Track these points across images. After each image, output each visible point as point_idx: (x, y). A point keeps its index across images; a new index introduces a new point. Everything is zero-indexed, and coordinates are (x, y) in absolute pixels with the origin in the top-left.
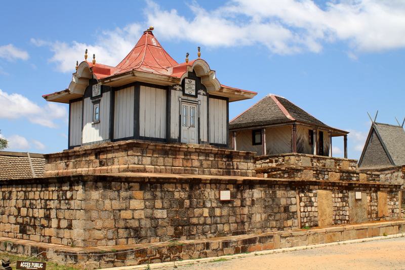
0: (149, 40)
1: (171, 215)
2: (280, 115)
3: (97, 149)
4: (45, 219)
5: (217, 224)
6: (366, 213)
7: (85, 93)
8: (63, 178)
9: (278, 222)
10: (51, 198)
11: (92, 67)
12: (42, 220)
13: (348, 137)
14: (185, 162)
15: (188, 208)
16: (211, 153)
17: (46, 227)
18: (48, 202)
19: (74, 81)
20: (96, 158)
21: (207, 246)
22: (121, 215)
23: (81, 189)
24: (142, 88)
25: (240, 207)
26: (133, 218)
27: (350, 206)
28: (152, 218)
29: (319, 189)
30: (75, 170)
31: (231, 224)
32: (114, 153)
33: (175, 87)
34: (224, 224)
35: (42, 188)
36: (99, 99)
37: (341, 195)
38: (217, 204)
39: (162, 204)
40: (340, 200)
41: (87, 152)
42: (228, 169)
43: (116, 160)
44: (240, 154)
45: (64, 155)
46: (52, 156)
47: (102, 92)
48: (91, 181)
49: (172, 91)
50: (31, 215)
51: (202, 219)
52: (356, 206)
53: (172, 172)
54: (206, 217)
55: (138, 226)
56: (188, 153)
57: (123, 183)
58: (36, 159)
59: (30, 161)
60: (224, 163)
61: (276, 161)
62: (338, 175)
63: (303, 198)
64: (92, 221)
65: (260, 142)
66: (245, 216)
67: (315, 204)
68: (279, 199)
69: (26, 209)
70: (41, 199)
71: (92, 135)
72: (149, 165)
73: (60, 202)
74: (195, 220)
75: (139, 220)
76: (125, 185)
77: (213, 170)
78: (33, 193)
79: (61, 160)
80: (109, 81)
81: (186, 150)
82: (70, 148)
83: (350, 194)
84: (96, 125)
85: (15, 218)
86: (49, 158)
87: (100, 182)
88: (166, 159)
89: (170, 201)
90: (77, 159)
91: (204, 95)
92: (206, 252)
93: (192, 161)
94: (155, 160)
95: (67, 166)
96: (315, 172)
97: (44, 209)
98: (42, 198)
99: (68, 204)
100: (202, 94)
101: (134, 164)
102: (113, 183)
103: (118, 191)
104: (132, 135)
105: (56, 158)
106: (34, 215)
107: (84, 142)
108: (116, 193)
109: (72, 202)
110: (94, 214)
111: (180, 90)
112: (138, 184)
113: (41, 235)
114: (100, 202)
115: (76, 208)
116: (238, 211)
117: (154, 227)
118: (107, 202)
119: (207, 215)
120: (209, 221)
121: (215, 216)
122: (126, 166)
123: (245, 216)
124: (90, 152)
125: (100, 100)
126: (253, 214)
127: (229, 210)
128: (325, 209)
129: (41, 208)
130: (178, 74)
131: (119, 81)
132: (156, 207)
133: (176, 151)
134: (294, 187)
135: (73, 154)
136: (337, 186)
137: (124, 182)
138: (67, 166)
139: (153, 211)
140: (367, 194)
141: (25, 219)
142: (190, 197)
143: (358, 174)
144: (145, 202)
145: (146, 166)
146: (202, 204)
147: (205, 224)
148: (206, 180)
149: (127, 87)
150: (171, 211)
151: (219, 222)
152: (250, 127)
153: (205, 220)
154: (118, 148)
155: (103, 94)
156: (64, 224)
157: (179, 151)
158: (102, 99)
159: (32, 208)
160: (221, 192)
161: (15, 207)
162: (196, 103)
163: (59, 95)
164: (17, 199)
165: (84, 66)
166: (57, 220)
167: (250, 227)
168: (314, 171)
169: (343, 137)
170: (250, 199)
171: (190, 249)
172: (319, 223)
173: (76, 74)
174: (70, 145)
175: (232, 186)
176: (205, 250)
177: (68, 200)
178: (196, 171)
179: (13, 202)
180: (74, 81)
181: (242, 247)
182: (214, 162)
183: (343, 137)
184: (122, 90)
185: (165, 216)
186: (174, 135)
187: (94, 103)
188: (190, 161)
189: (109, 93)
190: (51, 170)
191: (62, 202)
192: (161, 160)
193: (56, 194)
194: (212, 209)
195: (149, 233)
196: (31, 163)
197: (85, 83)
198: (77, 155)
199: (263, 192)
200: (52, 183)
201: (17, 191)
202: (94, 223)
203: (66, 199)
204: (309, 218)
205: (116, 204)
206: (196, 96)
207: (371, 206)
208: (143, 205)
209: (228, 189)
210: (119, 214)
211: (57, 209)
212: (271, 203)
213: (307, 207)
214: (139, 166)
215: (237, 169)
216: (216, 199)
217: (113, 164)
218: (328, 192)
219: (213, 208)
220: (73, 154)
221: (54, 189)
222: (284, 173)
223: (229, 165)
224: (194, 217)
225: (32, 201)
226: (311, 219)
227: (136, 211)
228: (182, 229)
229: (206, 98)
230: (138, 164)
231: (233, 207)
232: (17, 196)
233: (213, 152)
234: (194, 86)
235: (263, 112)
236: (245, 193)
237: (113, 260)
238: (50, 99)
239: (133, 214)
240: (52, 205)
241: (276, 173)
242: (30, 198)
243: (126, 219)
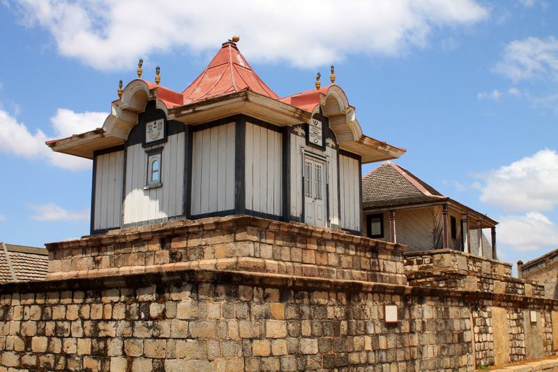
0: (234, 57)
1: (324, 348)
2: (413, 192)
3: (166, 230)
5: (382, 363)
6: (541, 344)
8: (113, 280)
9: (452, 359)
10: (108, 317)
11: (154, 89)
12: (86, 360)
13: (497, 230)
14: (318, 255)
15: (346, 336)
16: (351, 243)
18: (101, 325)
19: (115, 113)
20: (163, 247)
22: (254, 349)
23: (187, 297)
24: (249, 125)
25: (409, 333)
26: (271, 355)
27: (526, 332)
28: (298, 355)
29: (493, 306)
30: (114, 270)
32: (202, 237)
33: (296, 130)
34: (390, 363)
35: (85, 298)
36: (160, 146)
37: (515, 316)
38: (381, 328)
39: (312, 328)
41: (142, 237)
43: (208, 250)
44: (387, 247)
45: (89, 243)
46: (65, 246)
47: (168, 132)
48: (207, 282)
49: (292, 134)
50: (58, 351)
51: (364, 354)
56: (322, 241)
57: (255, 288)
58: (16, 254)
59: (8, 258)
60: (368, 260)
61: (419, 262)
63: (477, 320)
64: (210, 361)
65: (380, 233)
66: (416, 349)
67: (490, 329)
69: (45, 339)
70: (83, 320)
71: (142, 209)
73: (132, 325)
74: (354, 358)
75: (280, 357)
76: (258, 291)
78: (63, 308)
79: (84, 252)
80: (191, 110)
81: (320, 236)
82: (93, 231)
83: (525, 313)
84: (153, 192)
85: (17, 357)
86: (55, 249)
87: (220, 284)
88: (294, 249)
89: (322, 322)
90: (119, 251)
91: (333, 147)
93: (327, 255)
94: (278, 249)
95: (97, 263)
96: (479, 280)
97: (92, 338)
98: (86, 316)
99: (154, 327)
101: (249, 256)
102: (241, 287)
103: (249, 304)
104: (231, 206)
105: (75, 248)
106: (64, 350)
107: (127, 221)
108: (246, 306)
109: (164, 325)
110: (213, 347)
111: (302, 135)
112: (278, 290)
114: (222, 324)
115: (175, 335)
116: (406, 338)
118: (233, 322)
119: (370, 348)
121: (379, 350)
122: (233, 260)
123: (416, 349)
124: (150, 236)
125: (162, 148)
126: (424, 346)
127: (397, 340)
128: (501, 338)
129: (84, 337)
130: (309, 106)
131: (215, 109)
132: (303, 334)
134: (467, 301)
135: (113, 241)
136: (512, 302)
137: (257, 286)
139: (299, 341)
140: (542, 314)
141: (43, 358)
142: (347, 317)
143: (523, 284)
144: (287, 324)
145: (267, 261)
146: (362, 329)
148: (368, 286)
150: (323, 340)
151: (384, 360)
152: (371, 208)
153: (368, 356)
154: (214, 227)
155: (169, 137)
157: (311, 237)
158: (167, 146)
159: (62, 338)
160: (387, 307)
161: (19, 334)
162: (323, 159)
163: (81, 140)
164: (23, 320)
165: (136, 88)
166: (125, 361)
167: (422, 367)
168: (478, 277)
169: (490, 229)
170: (421, 321)
173: (117, 103)
174: (95, 228)
175: (398, 297)
178: (333, 272)
179: (14, 326)
180: (115, 113)
182: (355, 258)
183: (490, 229)
184: (209, 130)
185: (316, 351)
186: (295, 211)
187: (150, 153)
188: (325, 255)
189: (182, 136)
190: (60, 270)
192: (286, 251)
193: (123, 310)
194: (376, 337)
196: (9, 261)
197: (133, 119)
198: (119, 243)
199: (434, 309)
200: (111, 288)
201: (24, 306)
202: (212, 364)
203: (148, 318)
204: (484, 352)
205: (247, 328)
206: (323, 148)
208: (285, 330)
209: (393, 304)
210: (250, 348)
211: (124, 338)
212: (443, 327)
214: (256, 260)
215: (384, 271)
216: (380, 320)
217: (202, 256)
218: (503, 309)
219: (377, 335)
220: (113, 241)
221: (116, 299)
222: (438, 281)
223: (374, 263)
225: (60, 324)
226: (486, 354)
227: (276, 342)
229: (335, 151)
230: (255, 257)
231: (401, 334)
232: (23, 313)
233: (355, 241)
234: (321, 131)
235: (381, 188)
236: (413, 309)
238: (62, 147)
239: (271, 346)
241: (423, 280)
243: (261, 356)
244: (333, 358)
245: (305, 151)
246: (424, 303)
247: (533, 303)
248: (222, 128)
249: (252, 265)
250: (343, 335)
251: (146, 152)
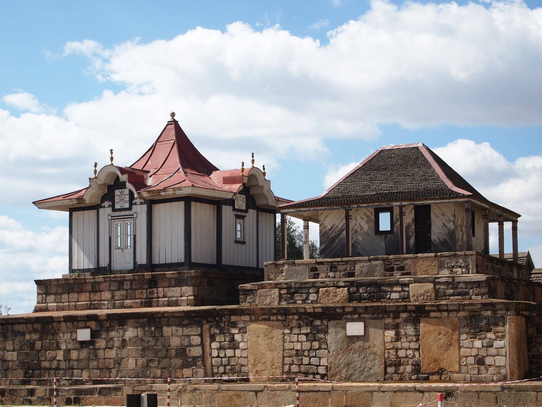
1: (21, 358)
5: (72, 369)
9: (165, 370)
21: (32, 392)
31: (92, 371)
33: (103, 205)
34: (82, 370)
40: (304, 338)
42: (150, 298)
52: (347, 350)
53: (76, 308)
54: (60, 360)
62: (343, 292)
66: (112, 360)
67: (242, 345)
72: (53, 303)
74: (45, 364)
77: (128, 302)
91: (141, 203)
92: (30, 400)
100: (138, 203)
111: (109, 206)
116: (101, 353)
117: (4, 370)
119: (61, 358)
120: (63, 365)
126: (123, 358)
127: (90, 353)
133: (81, 284)
146: (55, 346)
147: (58, 368)
150: (21, 353)
153: (58, 364)
170: (121, 339)
171: (13, 394)
172: (251, 377)
178: (104, 305)
181: (74, 398)
182: (129, 291)
185: (15, 359)
187: (237, 217)
194: (68, 352)
204: (228, 367)
206: (130, 209)
209: (86, 327)
212: (152, 343)
213: (224, 349)
224: (45, 360)
228: (32, 373)
230: (42, 303)
244: (28, 364)
245: (112, 217)
246: (125, 325)
247: (351, 313)
248: (175, 204)
249: (38, 308)
250: (37, 350)
251: (235, 215)
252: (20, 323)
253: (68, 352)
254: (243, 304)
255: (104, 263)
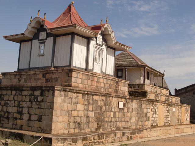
4: (18, 114)
5: (116, 122)
7: (33, 37)
17: (18, 119)
18: (21, 103)
24: (76, 37)
26: (78, 116)
43: (59, 79)
46: (6, 74)
55: (80, 121)
61: (134, 87)
65: (121, 76)
67: (157, 113)
68: (143, 109)
73: (32, 103)
74: (106, 119)
75: (81, 117)
78: (8, 96)
80: (56, 30)
97: (17, 107)
109: (42, 104)
113: (14, 124)
115: (46, 108)
116: (126, 114)
119: (113, 116)
123: (129, 118)
125: (45, 42)
129: (15, 106)
138: (20, 81)
146: (110, 110)
147: (111, 121)
149: (65, 35)
151: (117, 121)
152: (118, 67)
154: (61, 71)
156: (34, 117)
158: (47, 41)
159: (7, 106)
174: (19, 68)
176: (114, 138)
177: (39, 102)
185: (93, 116)
186: (90, 67)
189: (52, 38)
191: (34, 103)
194: (115, 113)
195: (85, 126)
203: (38, 101)
205: (70, 107)
206: (102, 46)
207: (179, 116)
210: (71, 113)
211: (29, 108)
223: (117, 87)
224: (107, 117)
225: (6, 101)
237: (71, 143)
240: (24, 104)
242: (4, 99)
243: (74, 117)
248: (67, 36)
251: (39, 43)
252: (96, 95)
253: (115, 113)
254: (126, 94)
255: (104, 71)
